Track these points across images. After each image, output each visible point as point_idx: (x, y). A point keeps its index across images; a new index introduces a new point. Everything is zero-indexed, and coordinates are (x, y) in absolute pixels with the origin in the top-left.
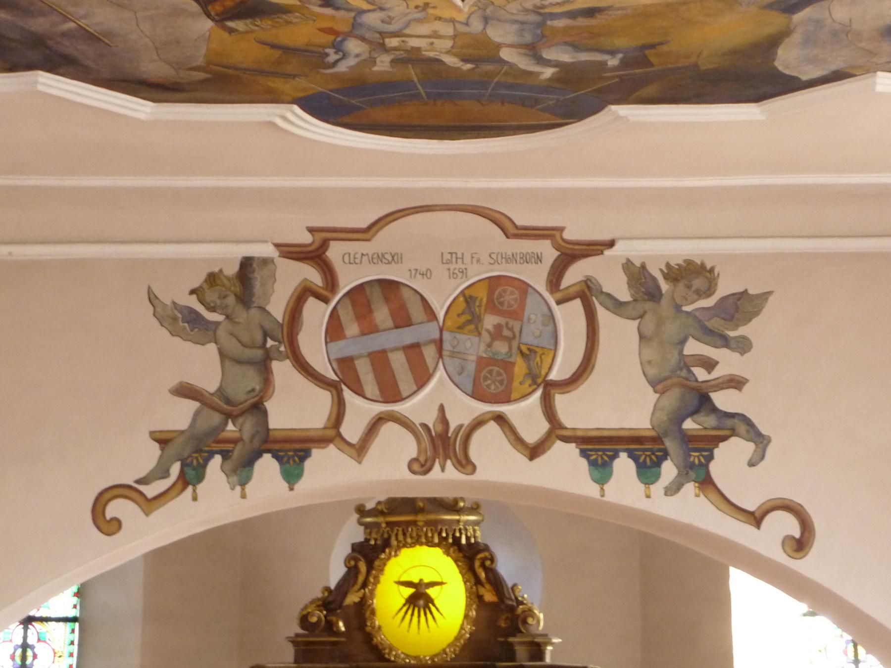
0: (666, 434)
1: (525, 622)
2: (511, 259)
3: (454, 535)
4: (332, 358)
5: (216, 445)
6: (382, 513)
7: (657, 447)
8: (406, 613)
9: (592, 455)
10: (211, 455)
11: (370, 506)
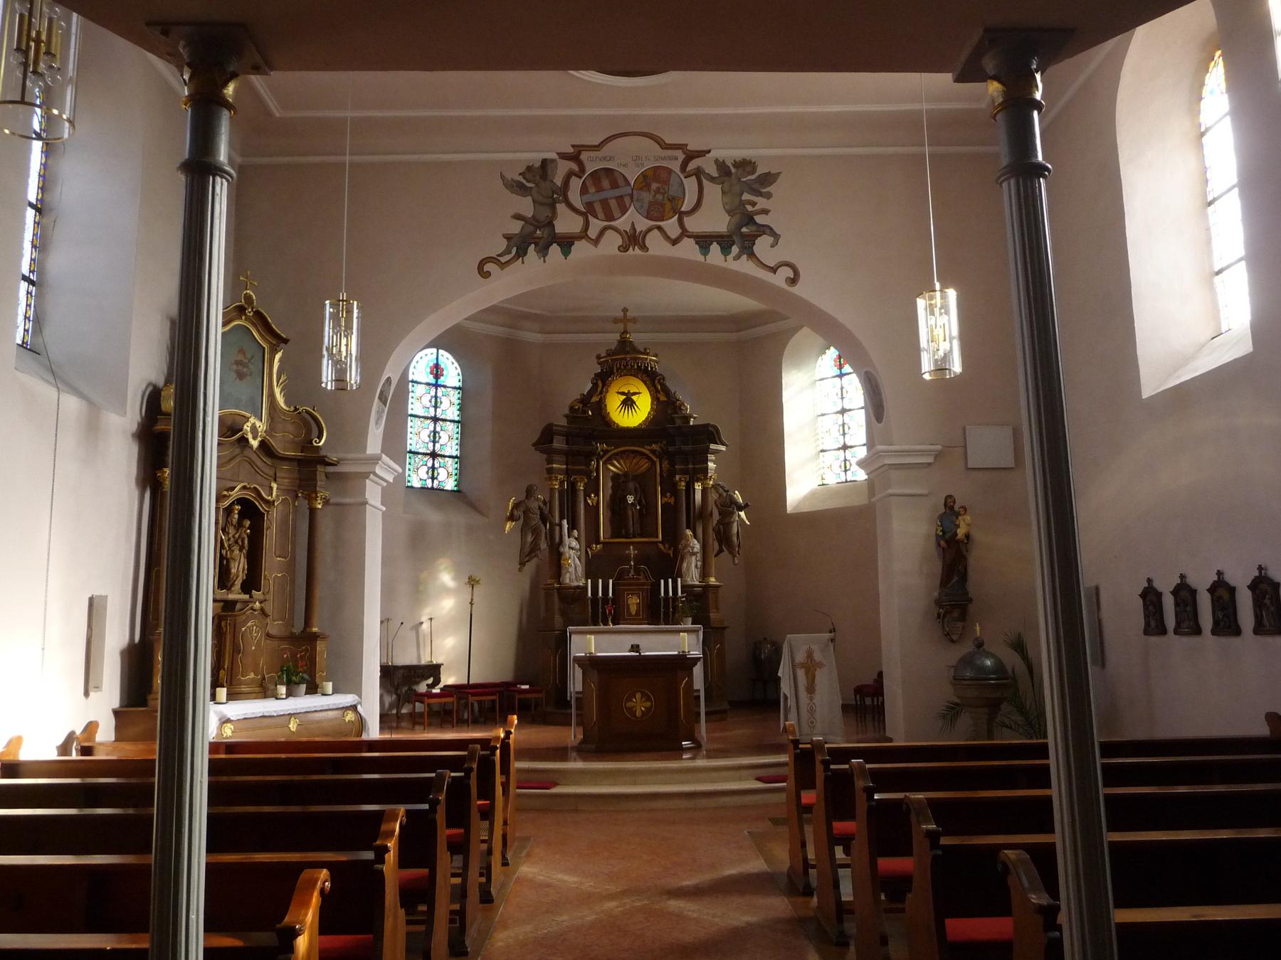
1: (681, 409)
10: (530, 244)
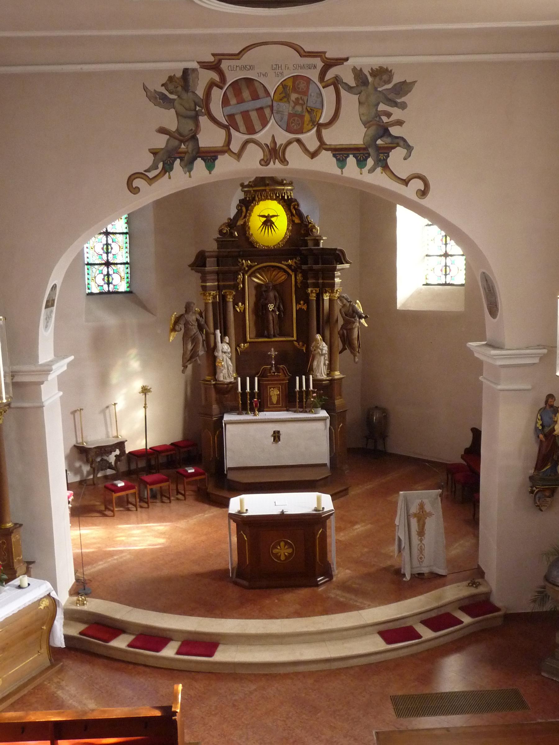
0: (369, 146)
1: (312, 231)
2: (302, 67)
3: (282, 196)
4: (225, 115)
5: (177, 154)
6: (251, 186)
7: (365, 152)
8: (263, 228)
9: (338, 156)
10: (175, 159)
11: (246, 183)
